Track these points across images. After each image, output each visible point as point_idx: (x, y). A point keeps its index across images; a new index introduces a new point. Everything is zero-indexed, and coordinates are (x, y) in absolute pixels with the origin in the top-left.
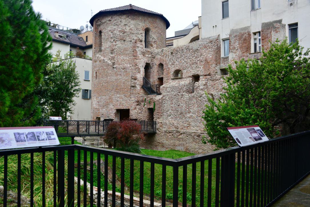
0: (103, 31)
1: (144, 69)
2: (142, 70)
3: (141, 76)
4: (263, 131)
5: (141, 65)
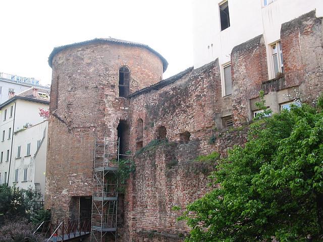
0: (61, 76)
1: (117, 131)
2: (114, 132)
3: (111, 139)
5: (111, 124)
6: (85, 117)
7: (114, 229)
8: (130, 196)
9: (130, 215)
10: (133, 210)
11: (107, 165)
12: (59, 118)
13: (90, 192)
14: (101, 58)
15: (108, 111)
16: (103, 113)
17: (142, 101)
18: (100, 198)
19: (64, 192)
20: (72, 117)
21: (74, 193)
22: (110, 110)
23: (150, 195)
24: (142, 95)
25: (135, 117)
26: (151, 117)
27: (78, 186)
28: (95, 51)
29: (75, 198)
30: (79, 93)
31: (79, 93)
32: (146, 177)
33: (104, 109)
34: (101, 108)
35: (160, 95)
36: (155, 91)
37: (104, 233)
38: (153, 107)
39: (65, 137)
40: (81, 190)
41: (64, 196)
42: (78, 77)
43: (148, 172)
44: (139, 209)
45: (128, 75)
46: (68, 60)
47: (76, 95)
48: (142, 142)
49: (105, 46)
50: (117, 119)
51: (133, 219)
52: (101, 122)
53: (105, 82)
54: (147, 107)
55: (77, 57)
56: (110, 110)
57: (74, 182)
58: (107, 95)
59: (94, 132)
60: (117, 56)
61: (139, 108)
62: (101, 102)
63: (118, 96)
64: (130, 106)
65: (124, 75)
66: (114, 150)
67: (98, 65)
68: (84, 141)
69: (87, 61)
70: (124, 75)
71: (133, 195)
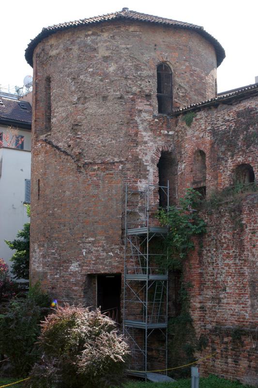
0: (56, 77)
1: (157, 169)
2: (152, 171)
3: (148, 184)
4: (147, 361)
5: (148, 158)
6: (104, 146)
7: (164, 325)
8: (193, 272)
9: (196, 303)
10: (200, 295)
11: (144, 225)
12: (57, 147)
13: (118, 267)
14: (127, 48)
15: (142, 137)
16: (134, 140)
17: (202, 121)
18: (132, 276)
19: (74, 267)
20: (82, 146)
21: (91, 269)
22: (146, 135)
23: (232, 270)
24: (202, 113)
25: (188, 147)
26: (223, 149)
27: (97, 258)
28: (117, 37)
29: (90, 277)
30: (92, 107)
31: (92, 107)
32: (223, 243)
33: (136, 134)
34: (132, 132)
35: (239, 114)
36: (225, 106)
37: (149, 330)
38: (225, 132)
39: (71, 178)
40: (102, 264)
41: (74, 274)
42: (90, 80)
43: (226, 235)
44: (209, 293)
45: (170, 76)
46: (68, 50)
47: (88, 110)
48: (205, 188)
49: (132, 29)
50: (158, 150)
51: (200, 308)
52: (132, 155)
53: (135, 89)
54: (214, 132)
55: (86, 45)
56: (146, 135)
57: (89, 252)
58: (140, 111)
59: (122, 170)
60: (152, 46)
61: (197, 134)
62: (130, 122)
63: (156, 113)
64: (177, 129)
65: (164, 74)
66: (152, 201)
67: (123, 60)
68: (106, 185)
69: (103, 52)
70: (164, 74)
71: (200, 271)
